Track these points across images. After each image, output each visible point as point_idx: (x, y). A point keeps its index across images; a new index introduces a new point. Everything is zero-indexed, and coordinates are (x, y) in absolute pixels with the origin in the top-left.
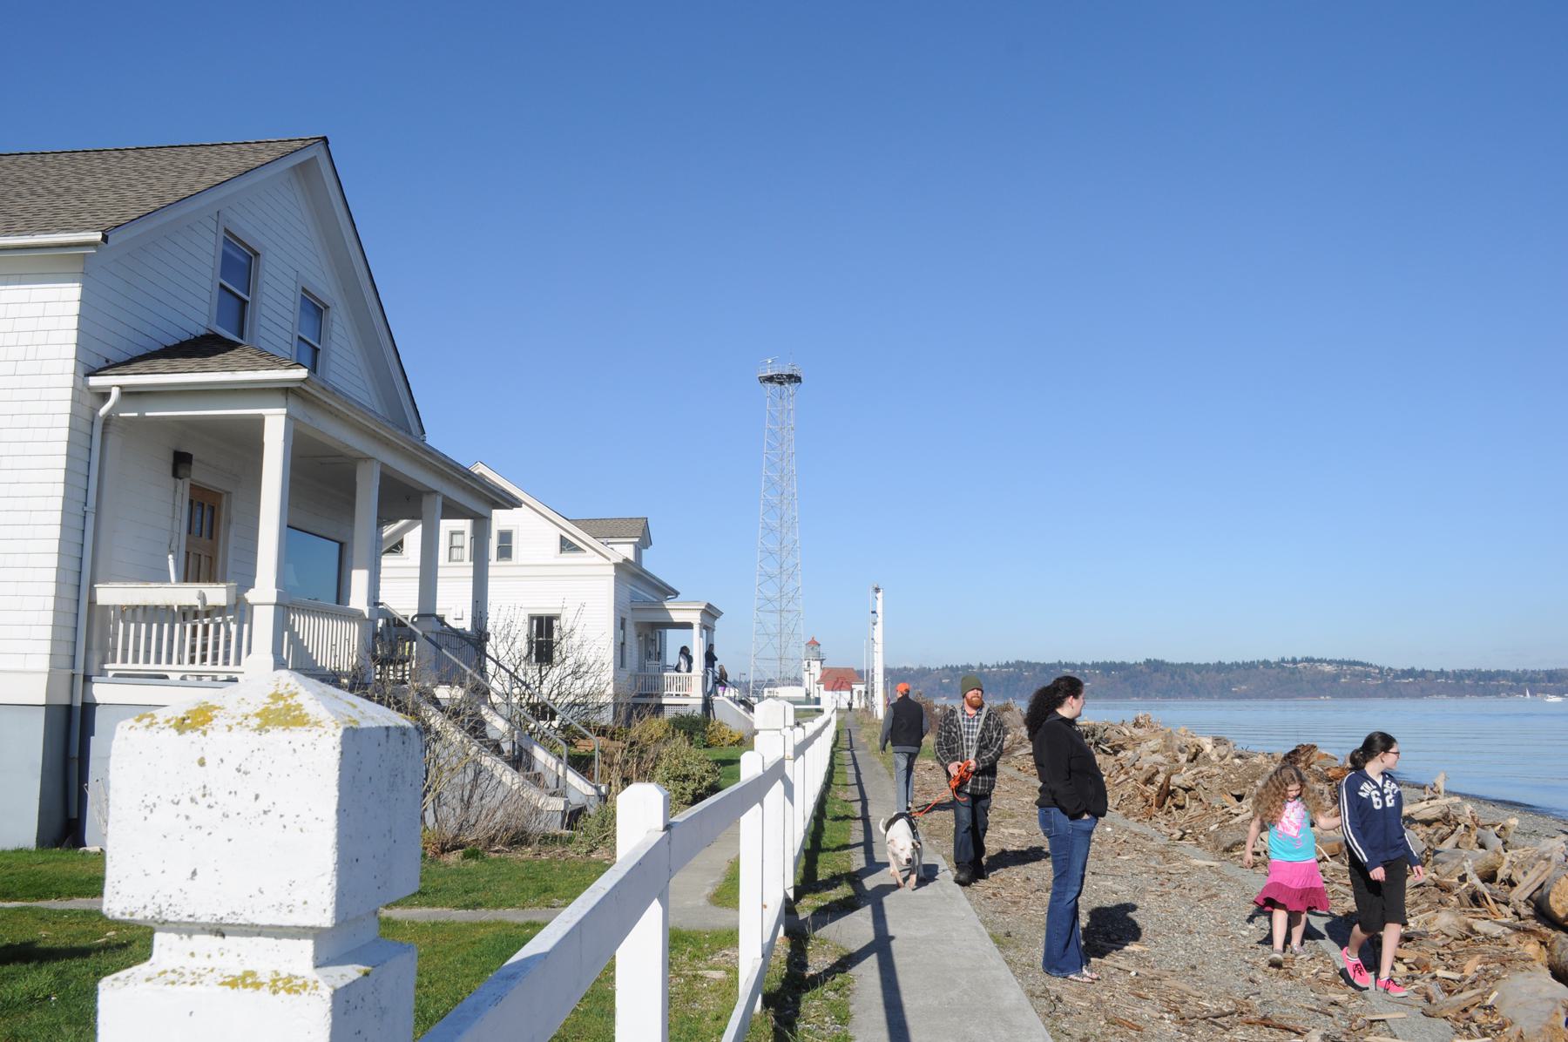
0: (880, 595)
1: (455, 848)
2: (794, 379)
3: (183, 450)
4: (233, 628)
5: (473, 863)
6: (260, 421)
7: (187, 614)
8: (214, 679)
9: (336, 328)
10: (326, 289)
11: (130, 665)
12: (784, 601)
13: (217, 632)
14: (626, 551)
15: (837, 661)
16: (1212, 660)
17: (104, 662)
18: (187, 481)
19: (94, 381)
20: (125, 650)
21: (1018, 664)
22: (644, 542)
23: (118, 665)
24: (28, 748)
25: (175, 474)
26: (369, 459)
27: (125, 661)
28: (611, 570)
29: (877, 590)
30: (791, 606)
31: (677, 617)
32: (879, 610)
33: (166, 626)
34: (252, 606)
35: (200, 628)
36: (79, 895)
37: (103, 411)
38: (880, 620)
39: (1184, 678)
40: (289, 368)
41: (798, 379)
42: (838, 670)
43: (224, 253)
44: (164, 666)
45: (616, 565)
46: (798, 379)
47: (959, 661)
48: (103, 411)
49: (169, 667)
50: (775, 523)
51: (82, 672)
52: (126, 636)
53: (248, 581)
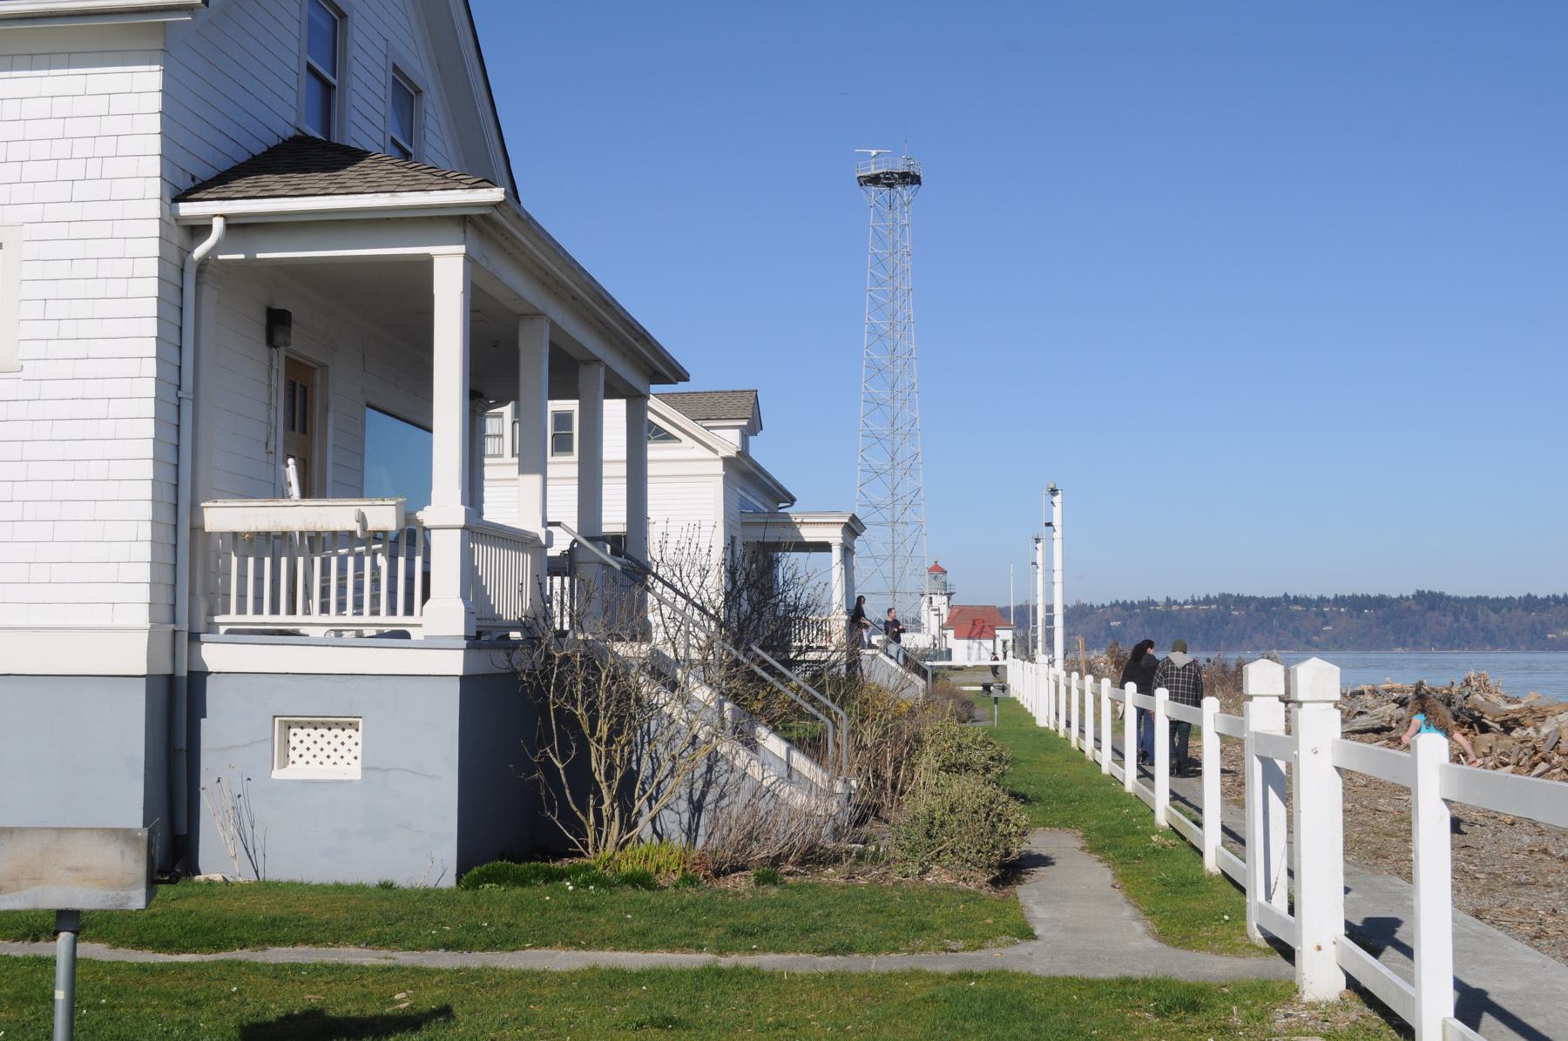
0: (1057, 499)
2: (910, 178)
3: (279, 306)
4: (382, 561)
5: (773, 892)
6: (426, 264)
7: (318, 541)
8: (360, 635)
9: (430, 123)
10: (420, 69)
11: (250, 617)
12: (899, 508)
13: (359, 566)
14: (729, 439)
15: (972, 595)
16: (1518, 593)
17: (211, 614)
18: (282, 350)
19: (187, 209)
20: (242, 596)
21: (1224, 599)
22: (753, 427)
23: (233, 617)
24: (127, 733)
25: (271, 342)
26: (538, 314)
27: (242, 610)
28: (718, 468)
29: (1054, 492)
31: (809, 534)
32: (1057, 522)
33: (267, 561)
34: (427, 530)
35: (334, 561)
36: (274, 942)
37: (199, 252)
38: (1058, 535)
39: (1474, 619)
40: (473, 187)
41: (915, 180)
42: (973, 609)
43: (310, 19)
44: (300, 617)
45: (727, 461)
46: (915, 180)
47: (1135, 596)
48: (199, 252)
49: (307, 619)
51: (186, 628)
52: (242, 577)
53: (418, 491)
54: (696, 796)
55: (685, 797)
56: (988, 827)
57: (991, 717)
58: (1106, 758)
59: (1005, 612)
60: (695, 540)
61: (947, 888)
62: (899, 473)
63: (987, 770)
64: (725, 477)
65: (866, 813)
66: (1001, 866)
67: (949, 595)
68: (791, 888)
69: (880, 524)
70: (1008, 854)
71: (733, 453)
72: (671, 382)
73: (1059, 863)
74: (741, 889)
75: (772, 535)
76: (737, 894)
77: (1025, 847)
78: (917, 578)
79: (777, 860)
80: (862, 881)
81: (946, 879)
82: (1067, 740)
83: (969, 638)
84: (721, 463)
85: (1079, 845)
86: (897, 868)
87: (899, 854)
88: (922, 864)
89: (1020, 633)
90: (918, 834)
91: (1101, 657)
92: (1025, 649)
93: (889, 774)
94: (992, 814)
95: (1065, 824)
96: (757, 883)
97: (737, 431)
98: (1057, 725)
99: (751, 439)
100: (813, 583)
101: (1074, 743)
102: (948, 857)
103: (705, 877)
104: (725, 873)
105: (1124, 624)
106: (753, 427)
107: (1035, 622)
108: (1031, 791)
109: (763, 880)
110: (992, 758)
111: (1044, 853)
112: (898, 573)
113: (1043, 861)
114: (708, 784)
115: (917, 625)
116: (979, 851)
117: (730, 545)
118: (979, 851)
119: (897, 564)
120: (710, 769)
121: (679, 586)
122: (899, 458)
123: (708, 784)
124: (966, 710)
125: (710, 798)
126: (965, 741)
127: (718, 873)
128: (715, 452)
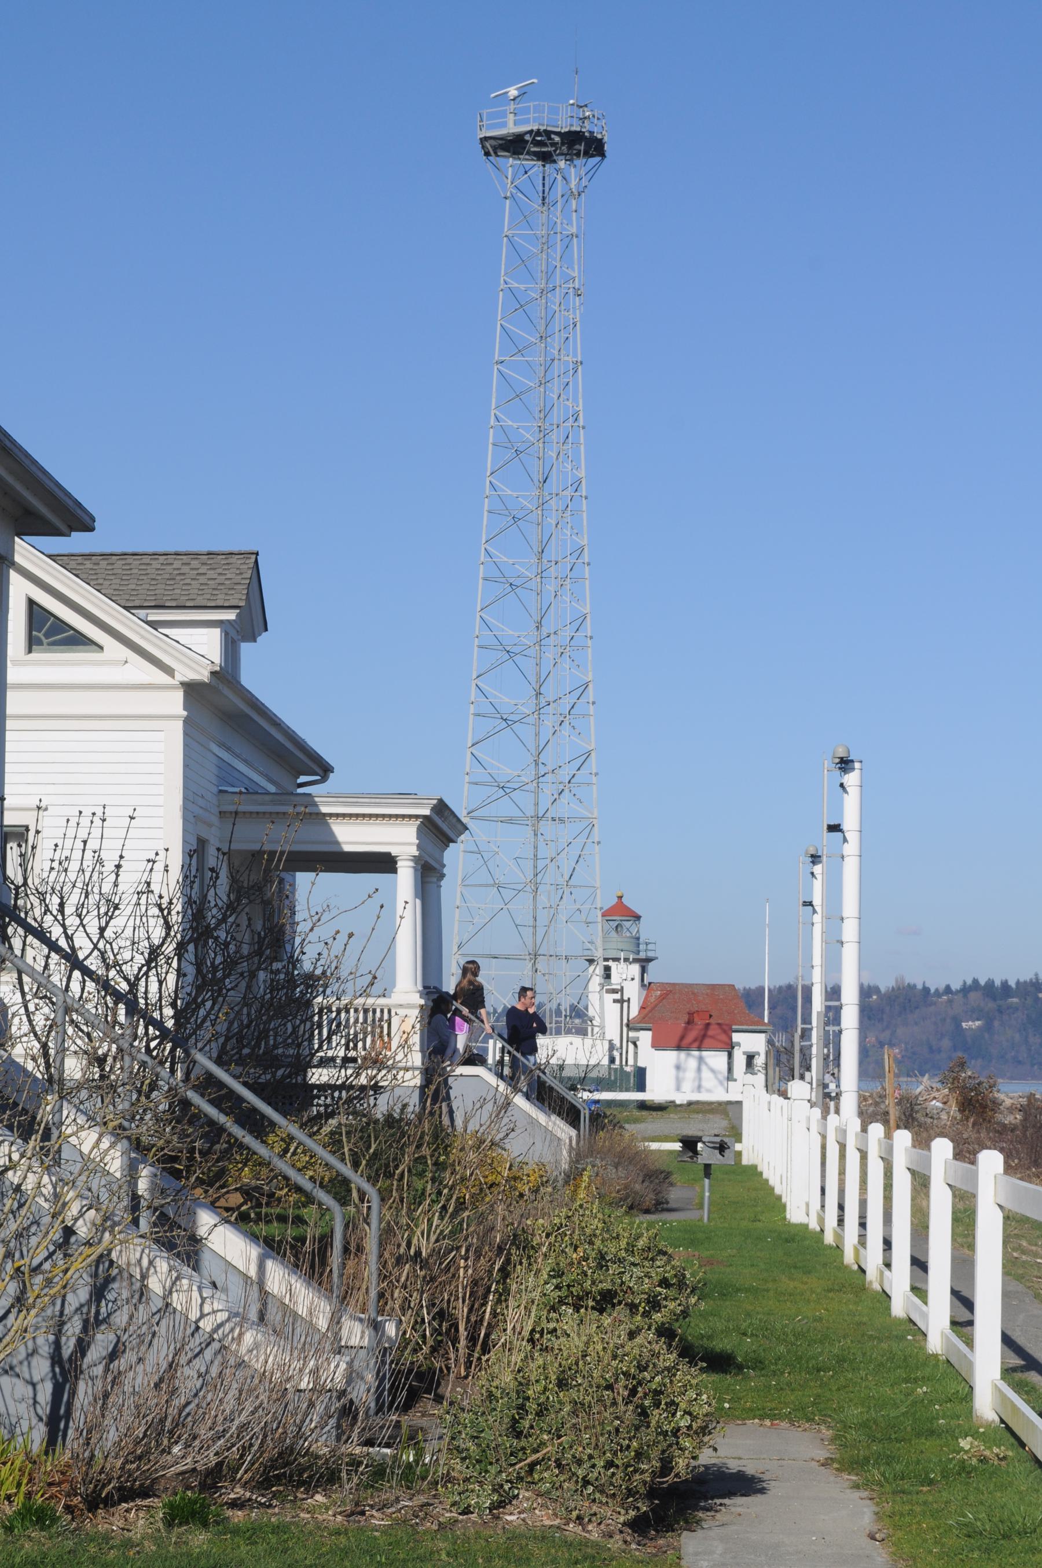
0: (851, 779)
1: (127, 1494)
2: (584, 145)
5: (199, 1539)
12: (548, 791)
14: (200, 647)
15: (691, 961)
22: (248, 624)
28: (175, 703)
29: (845, 764)
30: (566, 806)
31: (352, 837)
32: (851, 822)
38: (851, 849)
41: (595, 147)
42: (688, 991)
45: (191, 689)
46: (595, 147)
50: (525, 567)
54: (68, 1348)
55: (45, 1350)
56: (630, 1414)
57: (696, 1201)
58: (899, 1281)
59: (752, 998)
60: (93, 844)
61: (543, 1536)
62: (549, 722)
63: (654, 1304)
64: (187, 722)
65: (411, 1384)
66: (652, 1493)
67: (644, 963)
68: (236, 1532)
69: (510, 821)
70: (666, 1466)
71: (202, 674)
72: (57, 533)
73: (775, 1489)
74: (136, 1535)
75: (283, 838)
76: (128, 1544)
77: (706, 1457)
78: (582, 931)
79: (213, 1478)
80: (378, 1520)
81: (545, 1518)
82: (839, 1248)
83: (679, 1048)
84: (179, 695)
85: (822, 1454)
86: (449, 1496)
87: (459, 1468)
88: (497, 1488)
89: (780, 1040)
90: (495, 1431)
91: (936, 1097)
92: (784, 1066)
93: (461, 1311)
94: (643, 1396)
95: (802, 1414)
96: (169, 1524)
97: (216, 633)
98: (821, 1220)
99: (245, 648)
100: (324, 931)
101: (849, 1257)
102: (548, 1475)
103: (68, 1509)
104: (109, 1502)
105: (988, 1027)
106: (248, 624)
107: (807, 1019)
108: (741, 1347)
109: (181, 1515)
110: (664, 1283)
111: (750, 1470)
112: (543, 918)
113: (745, 1485)
114: (92, 1324)
115: (578, 1021)
116: (610, 1464)
117: (196, 852)
118: (610, 1464)
119: (543, 899)
120: (98, 1293)
121: (56, 932)
122: (549, 692)
123: (92, 1324)
124: (648, 1191)
125: (96, 1352)
126: (611, 1249)
127: (95, 1502)
128: (169, 671)
